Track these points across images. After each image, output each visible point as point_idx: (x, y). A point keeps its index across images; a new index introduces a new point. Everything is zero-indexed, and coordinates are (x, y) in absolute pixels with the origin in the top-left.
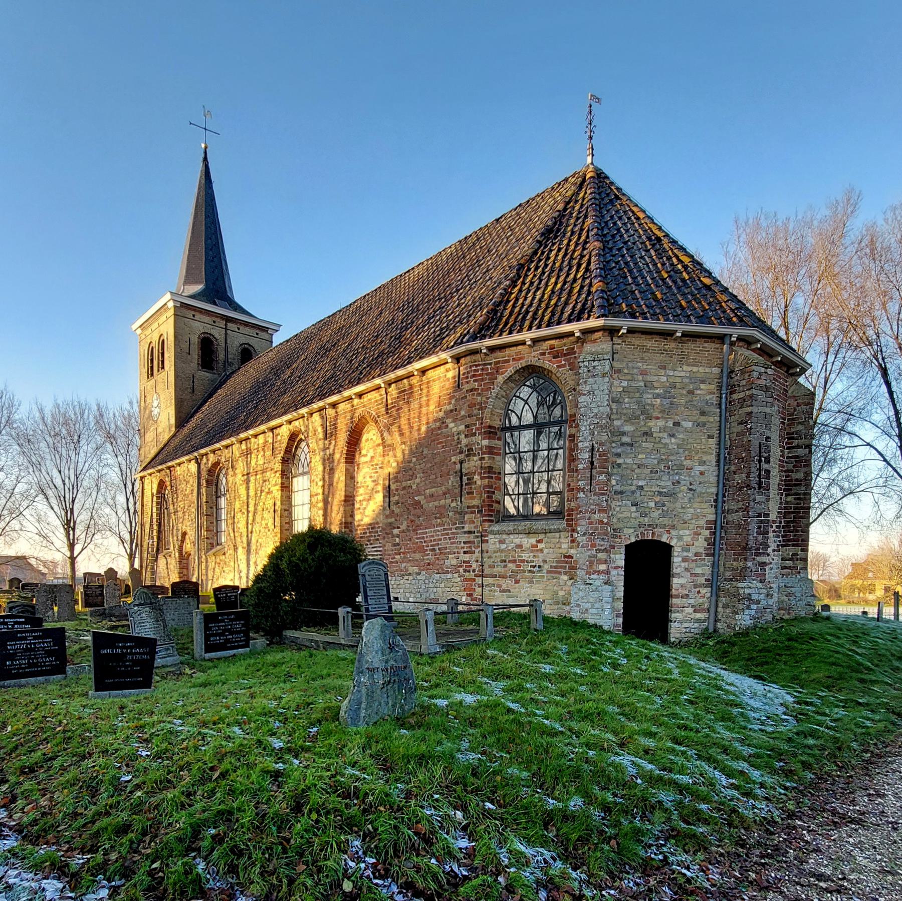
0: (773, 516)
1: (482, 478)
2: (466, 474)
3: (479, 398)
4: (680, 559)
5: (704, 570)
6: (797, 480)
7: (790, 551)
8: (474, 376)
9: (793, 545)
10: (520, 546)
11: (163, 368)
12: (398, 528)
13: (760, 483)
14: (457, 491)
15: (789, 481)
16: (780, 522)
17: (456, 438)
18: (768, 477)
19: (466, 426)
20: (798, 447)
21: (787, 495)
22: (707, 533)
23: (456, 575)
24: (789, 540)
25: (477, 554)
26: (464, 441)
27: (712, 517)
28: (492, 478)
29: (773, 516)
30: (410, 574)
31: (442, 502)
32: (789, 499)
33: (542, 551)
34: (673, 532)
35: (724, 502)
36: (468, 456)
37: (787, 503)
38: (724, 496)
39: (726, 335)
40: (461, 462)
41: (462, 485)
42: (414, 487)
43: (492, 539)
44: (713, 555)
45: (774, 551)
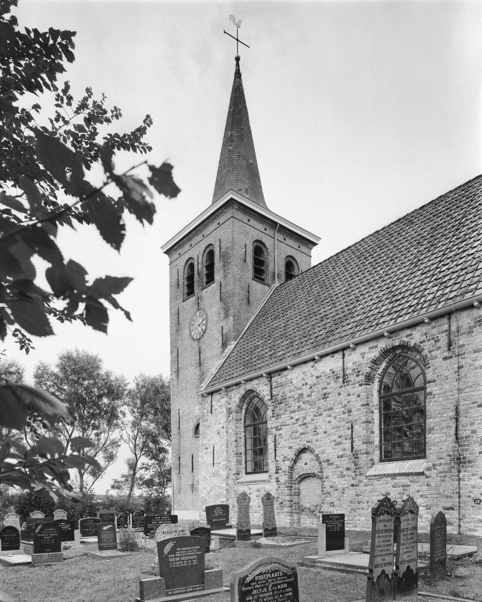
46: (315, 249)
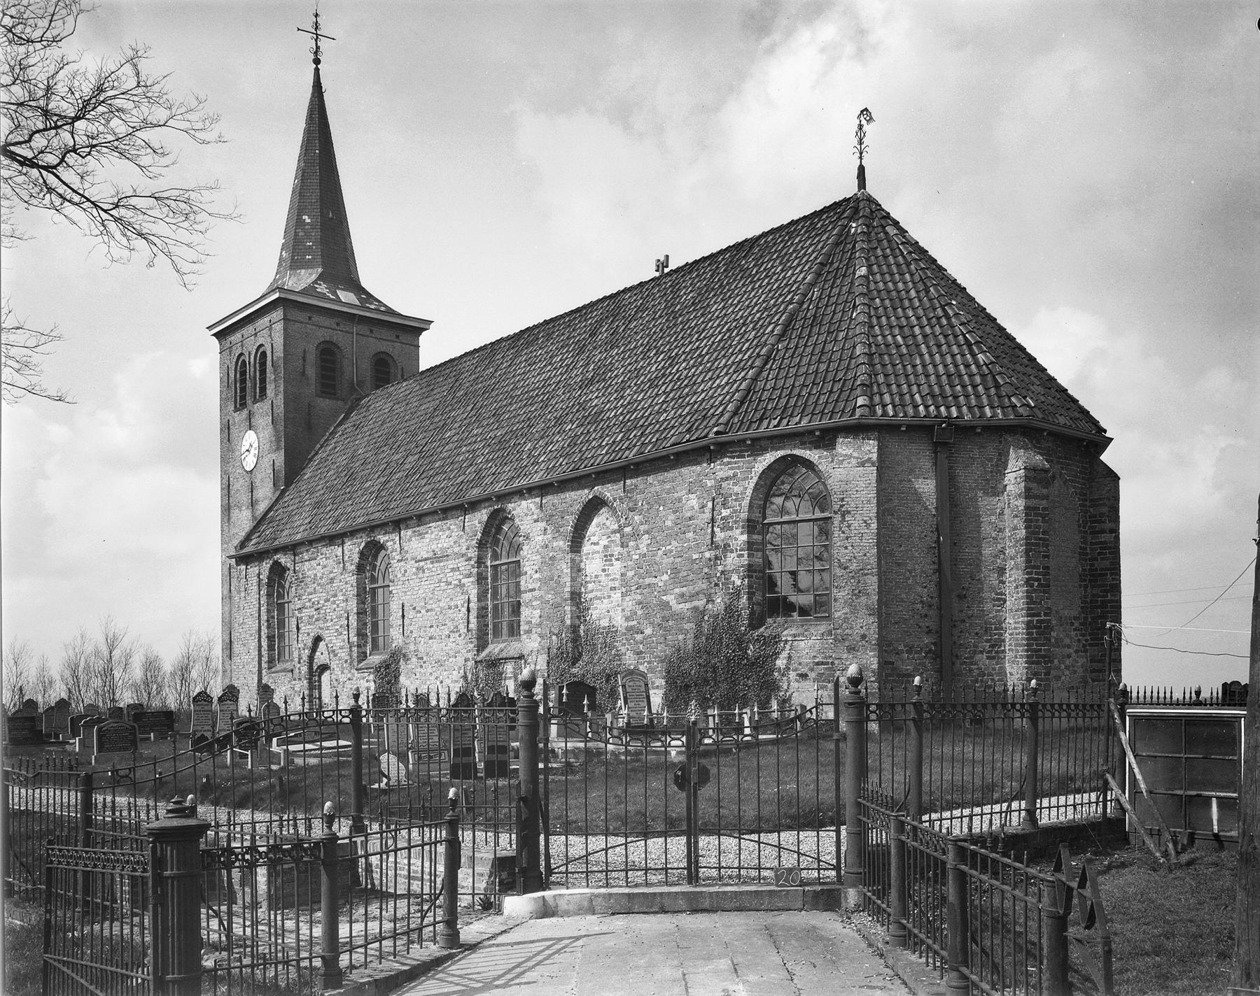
11: (263, 390)
20: (1103, 532)
46: (424, 333)
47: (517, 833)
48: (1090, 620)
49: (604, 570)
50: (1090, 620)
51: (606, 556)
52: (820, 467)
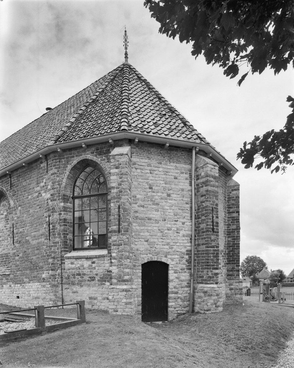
0: (221, 248)
1: (60, 226)
2: (52, 224)
3: (58, 178)
4: (173, 271)
5: (185, 276)
6: (233, 229)
7: (231, 266)
8: (55, 166)
9: (232, 263)
10: (83, 266)
12: (18, 256)
13: (213, 229)
14: (47, 233)
15: (229, 230)
16: (226, 252)
17: (46, 202)
18: (217, 226)
19: (51, 195)
20: (233, 212)
21: (228, 237)
22: (187, 257)
23: (48, 283)
24: (230, 261)
25: (59, 271)
26: (50, 203)
27: (189, 248)
28: (66, 225)
29: (221, 248)
30: (24, 283)
31: (40, 240)
32: (229, 239)
33: (95, 268)
34: (169, 256)
35: (195, 240)
36: (52, 212)
37: (228, 241)
38: (195, 236)
39: (193, 147)
40: (49, 216)
41: (50, 230)
42: (26, 231)
43: (67, 262)
44: (190, 269)
45: (223, 266)
47: (171, 32)
48: (227, 252)
49: (5, 227)
50: (227, 252)
51: (6, 220)
52: (101, 165)
